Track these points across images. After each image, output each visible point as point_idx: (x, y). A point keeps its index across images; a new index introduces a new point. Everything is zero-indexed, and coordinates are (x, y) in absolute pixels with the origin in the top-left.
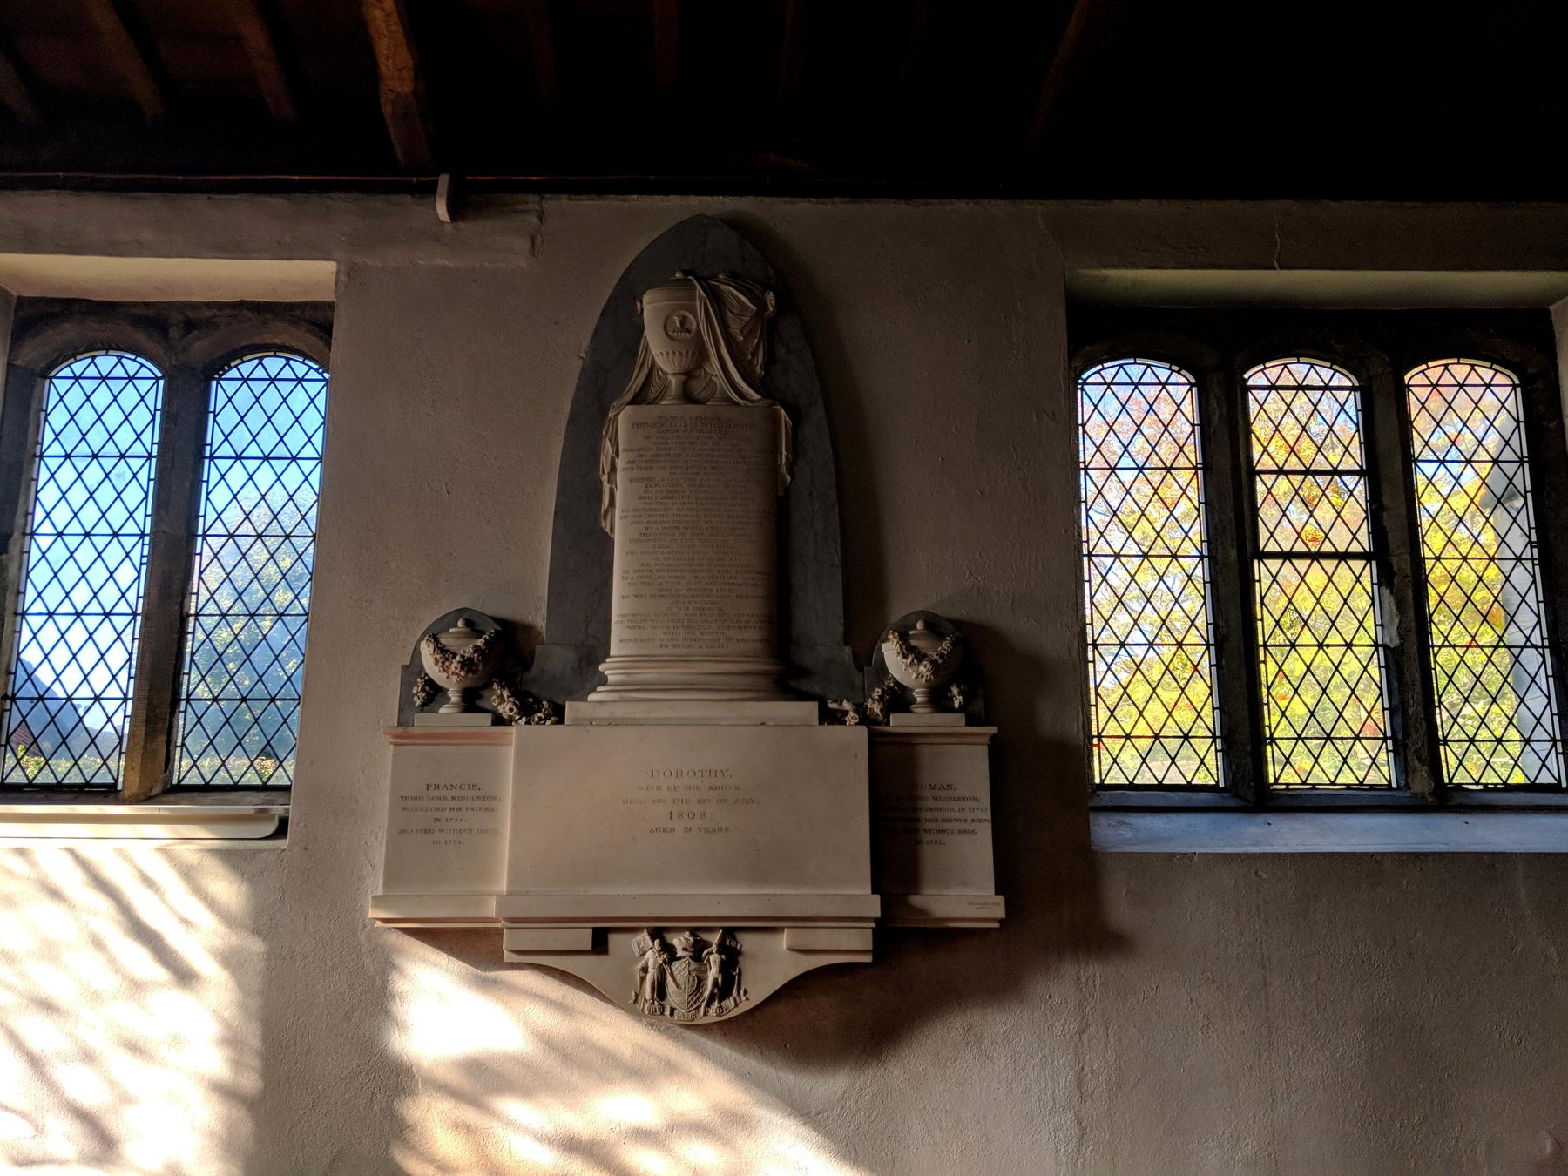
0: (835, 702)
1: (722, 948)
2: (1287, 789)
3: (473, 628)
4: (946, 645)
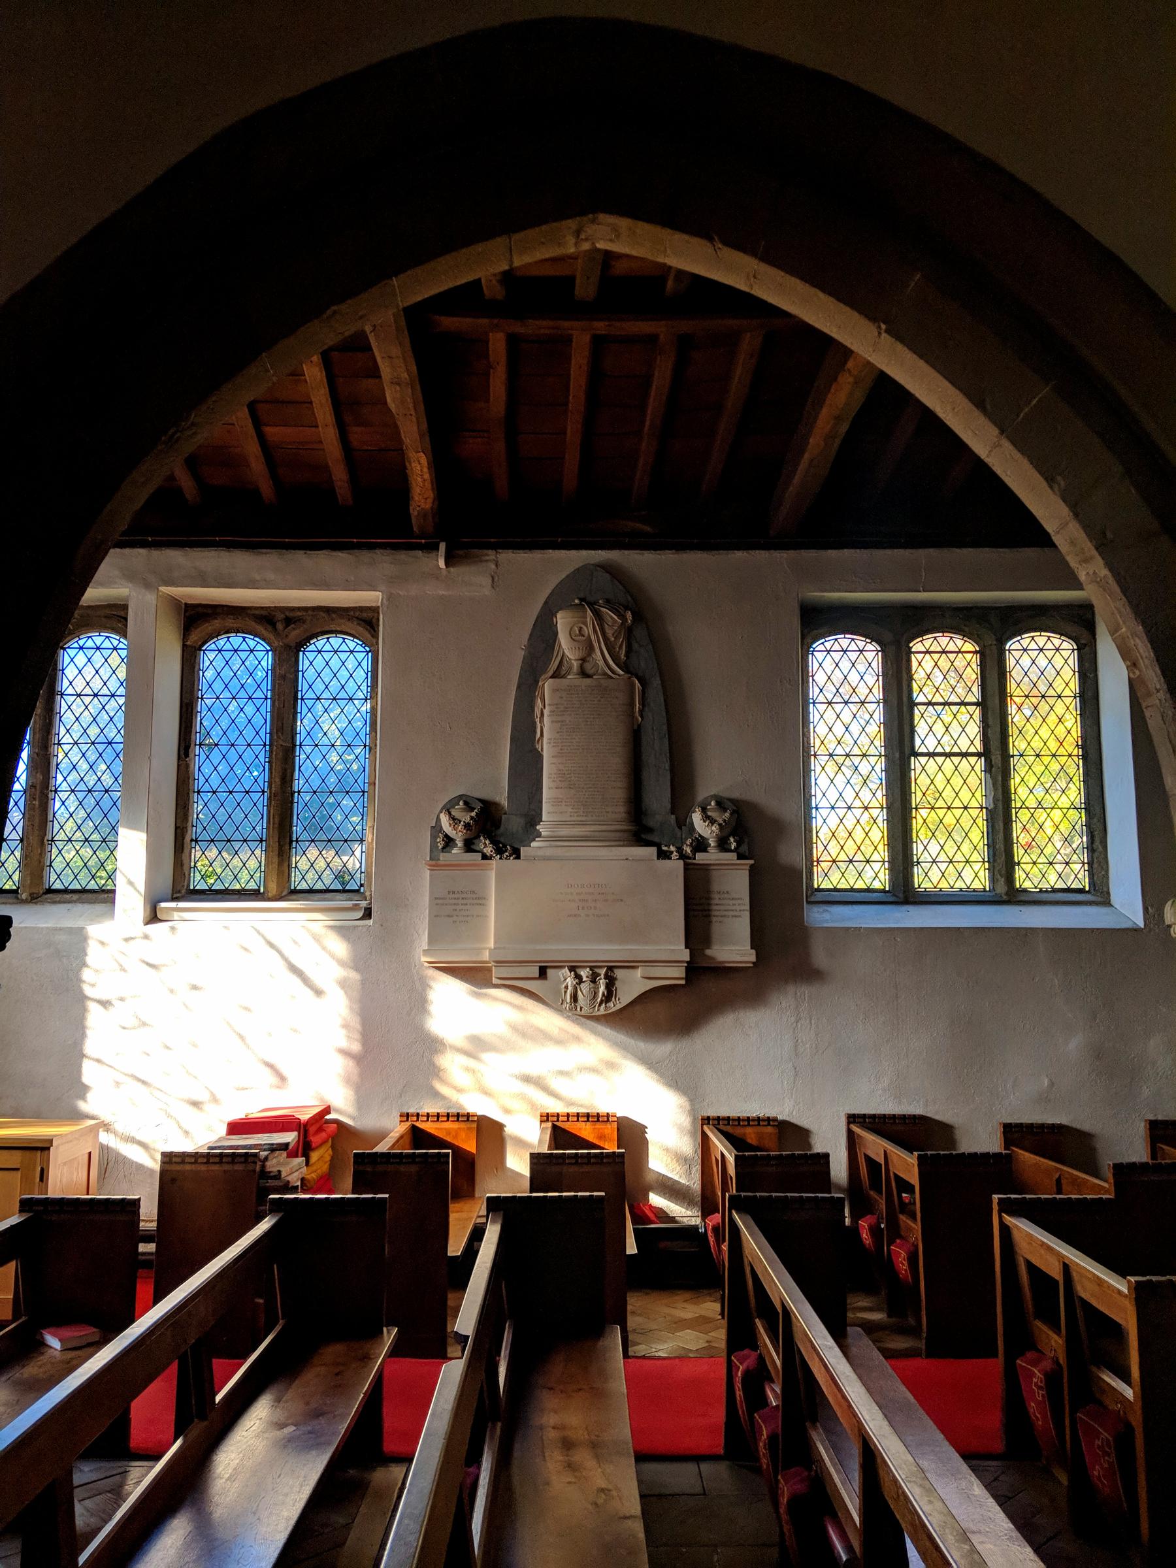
0: (666, 846)
1: (606, 976)
2: (925, 891)
3: (469, 807)
4: (727, 815)
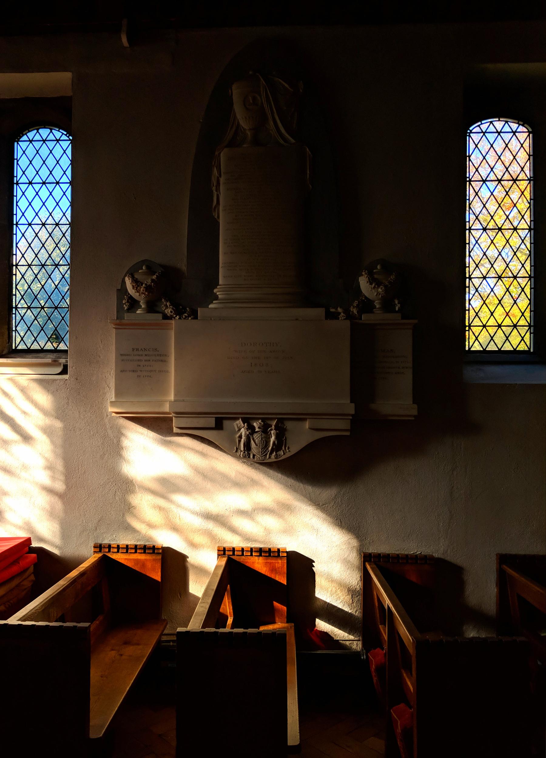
3: (150, 270)
4: (393, 277)
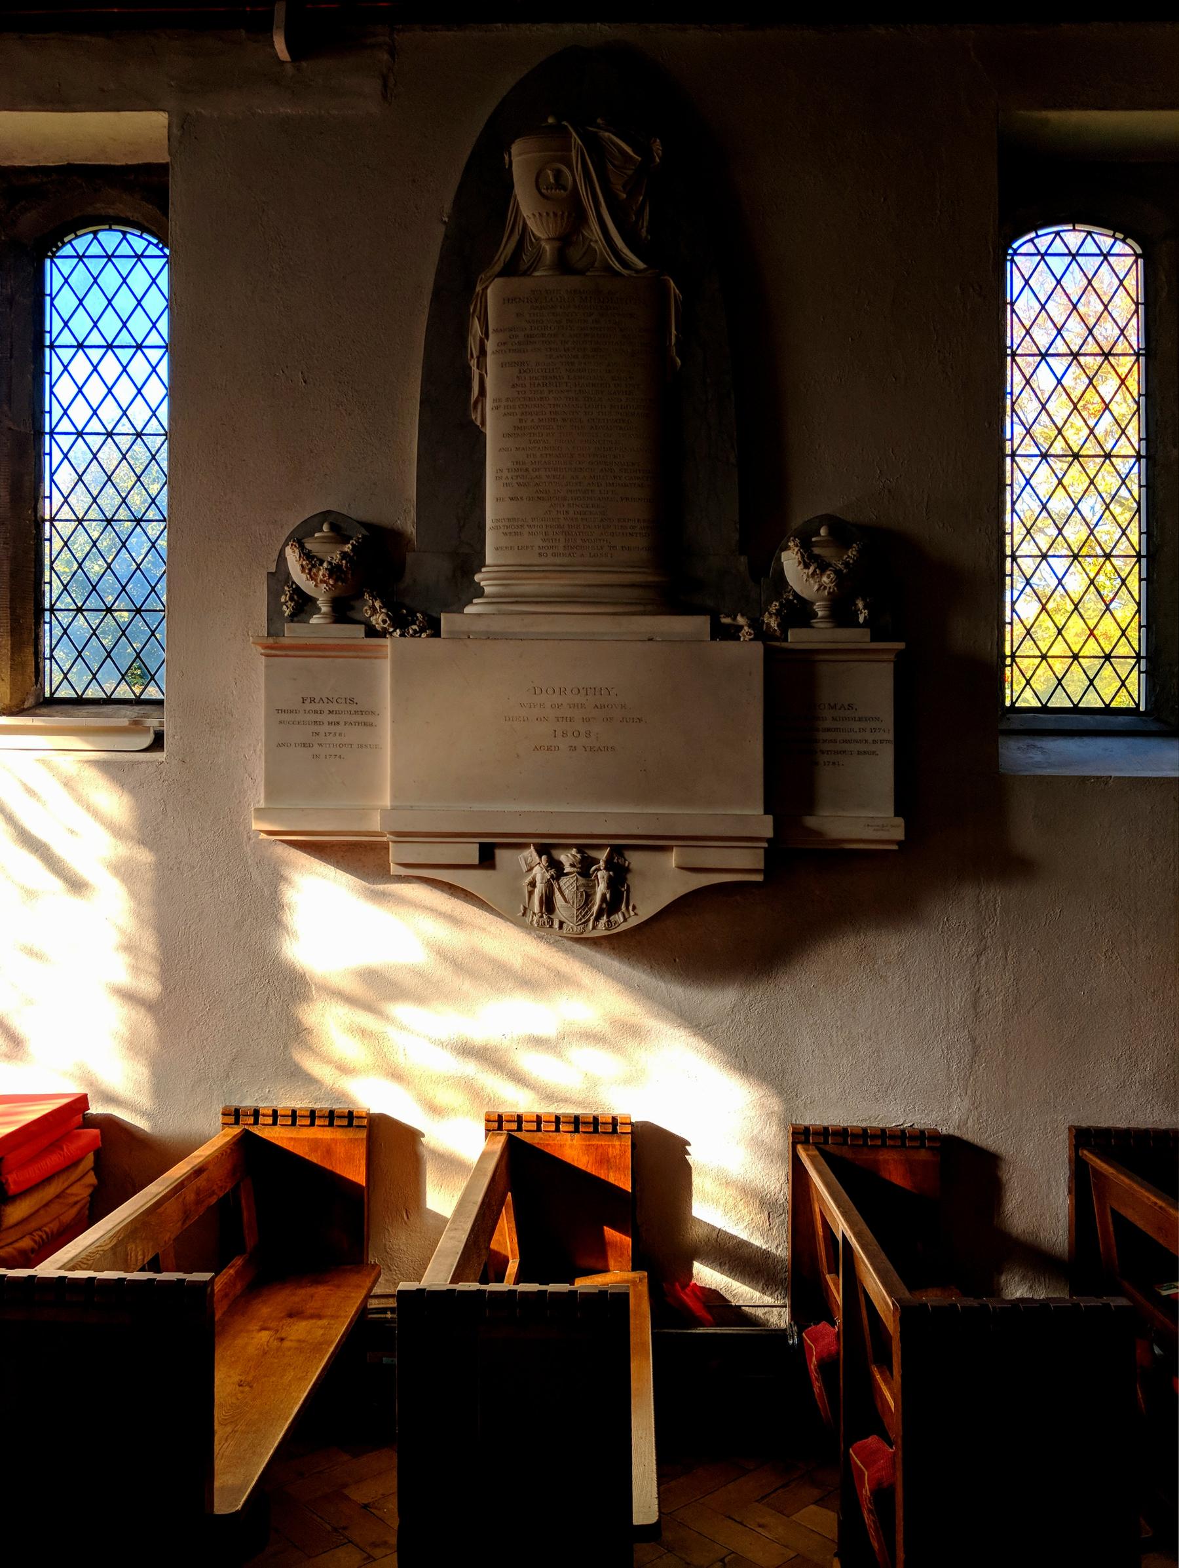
0: (727, 616)
1: (609, 865)
3: (339, 533)
